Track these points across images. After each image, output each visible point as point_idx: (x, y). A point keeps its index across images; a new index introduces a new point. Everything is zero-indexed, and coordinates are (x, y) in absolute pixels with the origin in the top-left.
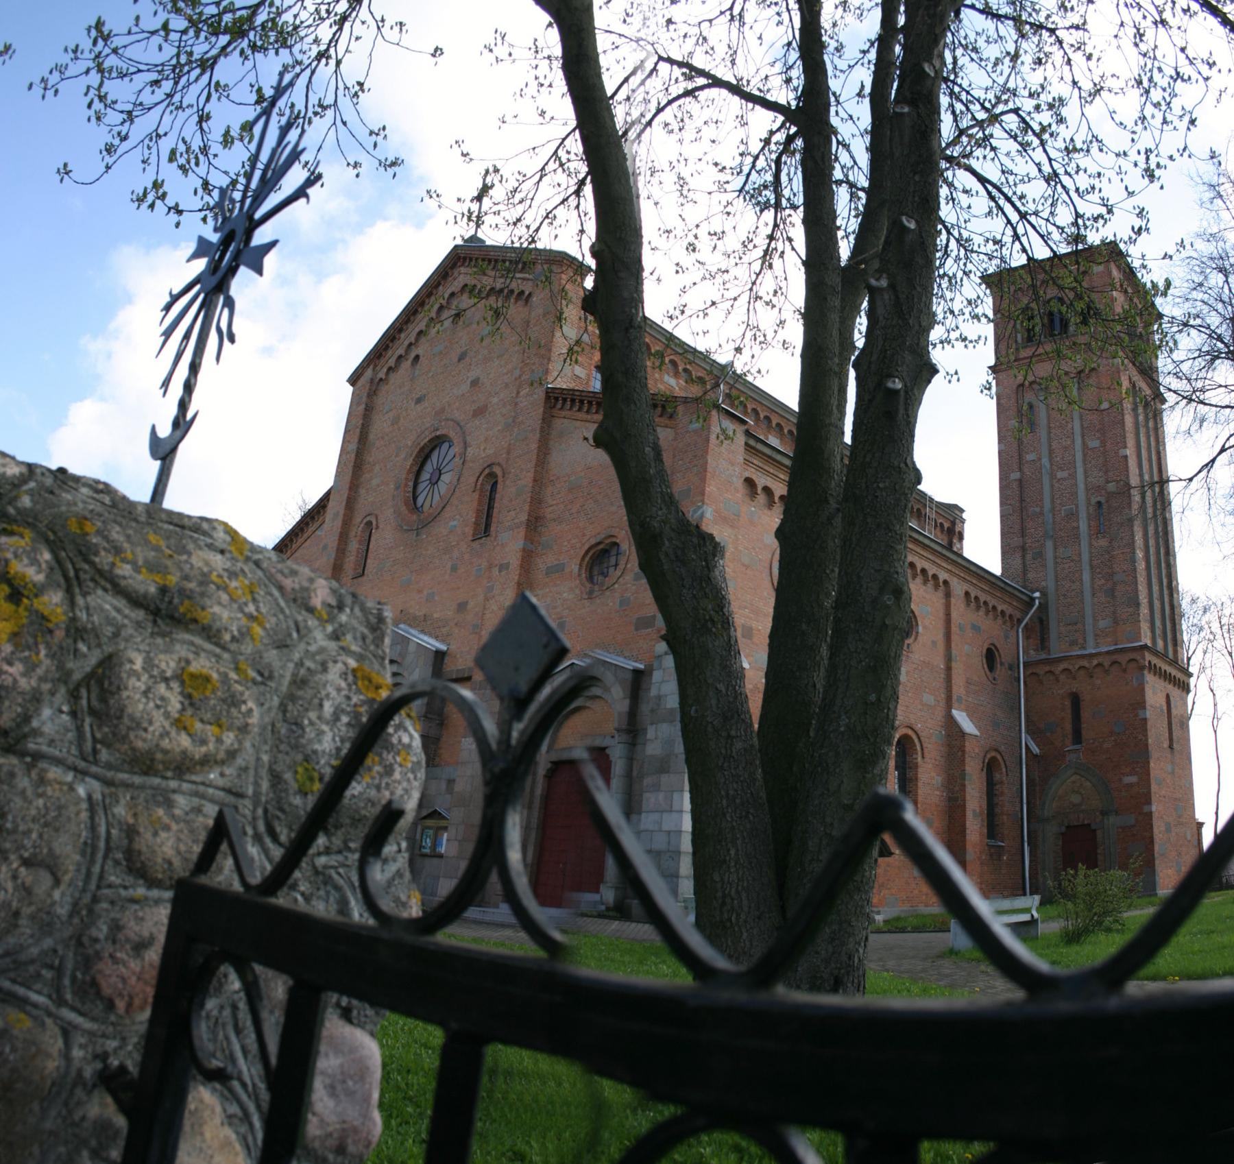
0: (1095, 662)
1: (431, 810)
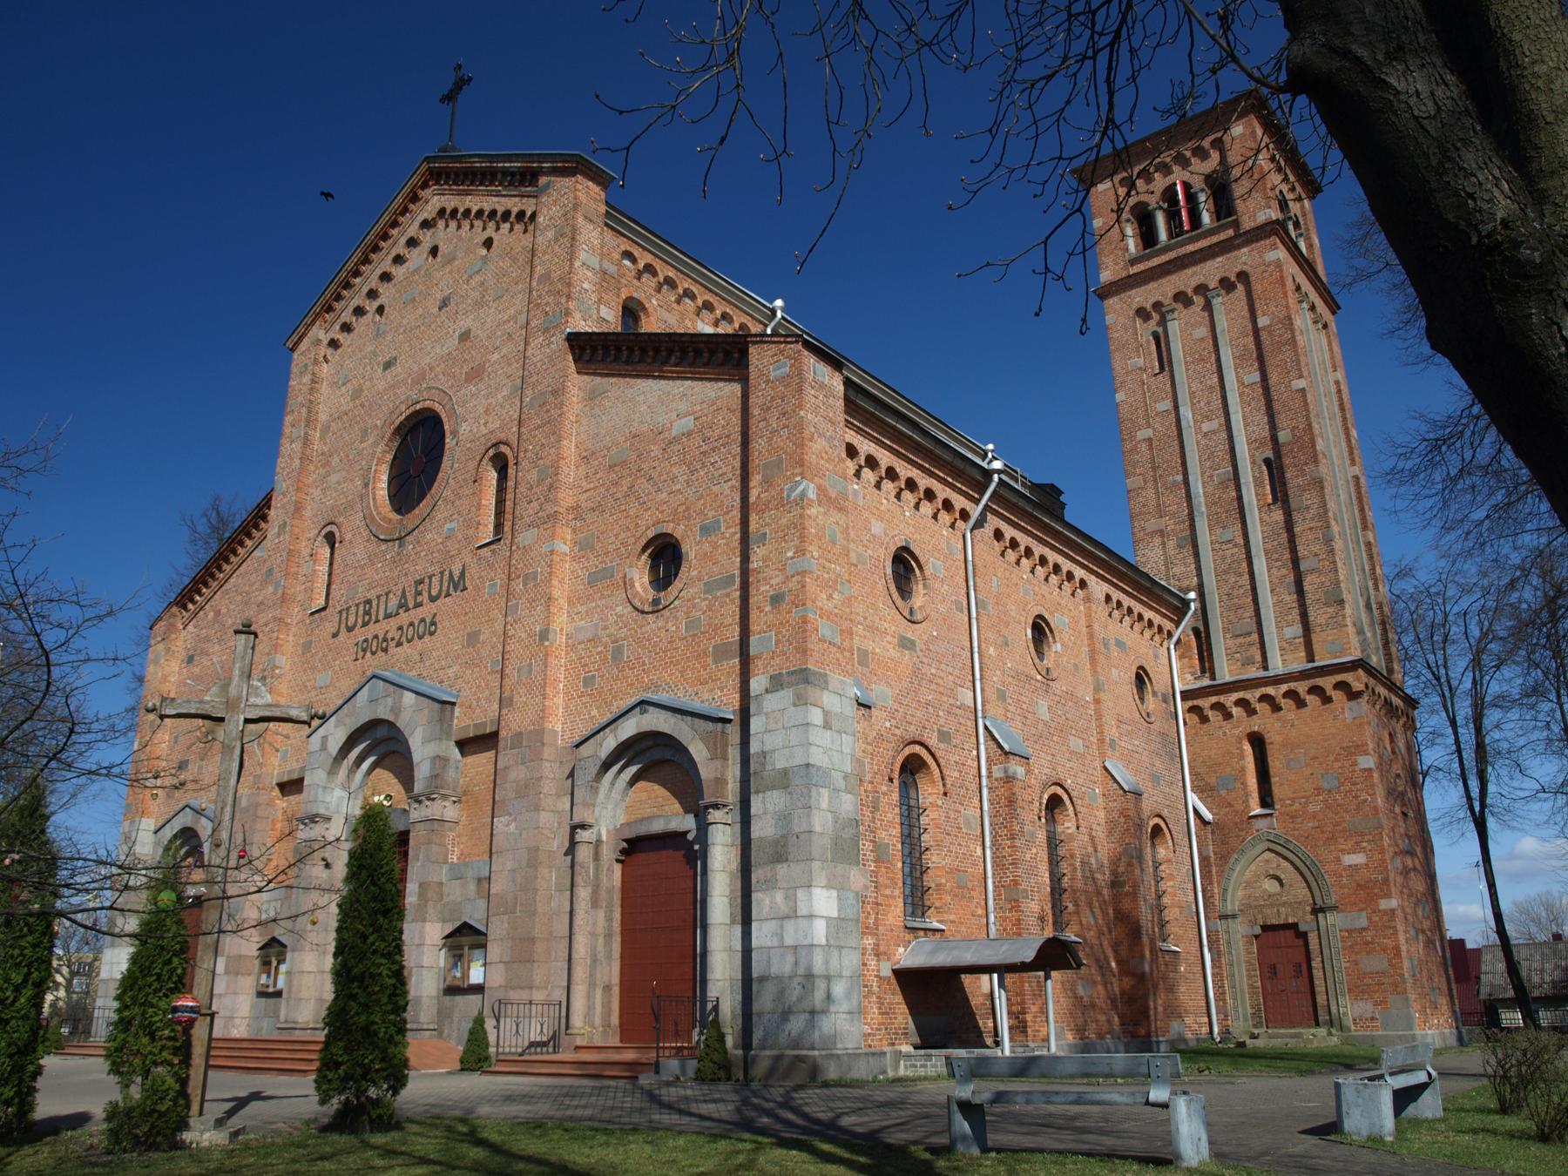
1: (458, 924)
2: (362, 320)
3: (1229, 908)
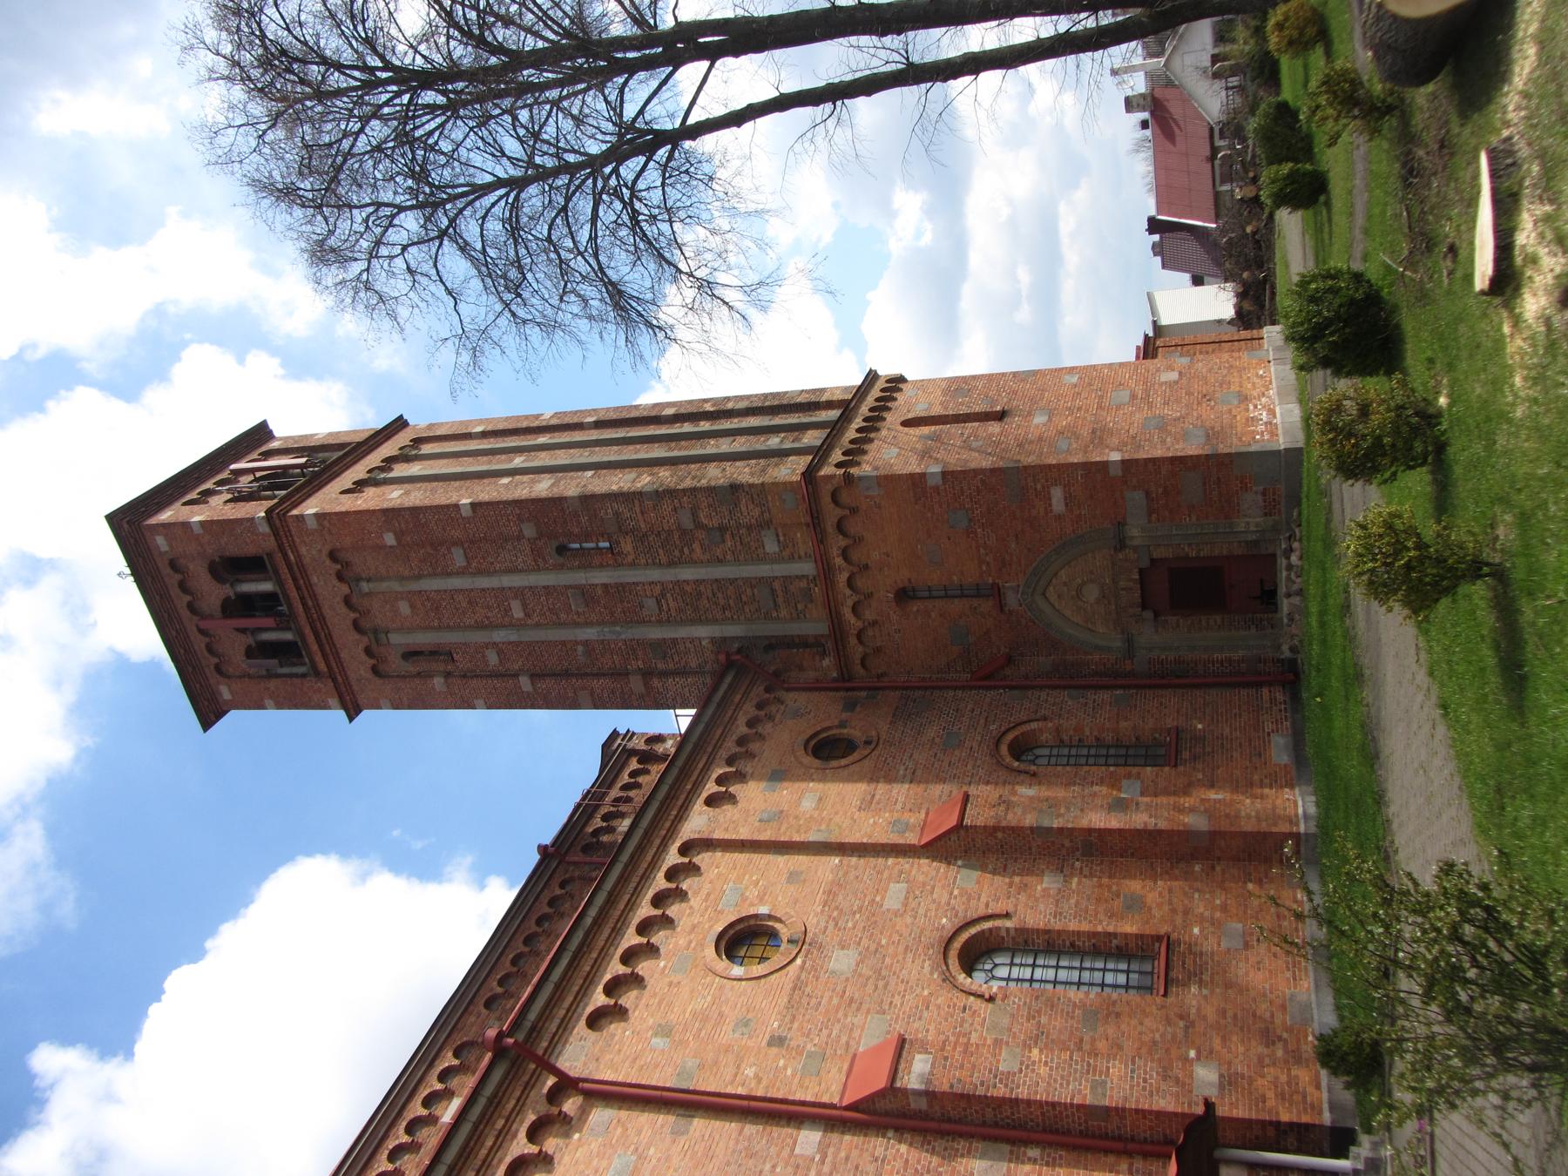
0: (839, 561)
3: (1117, 643)
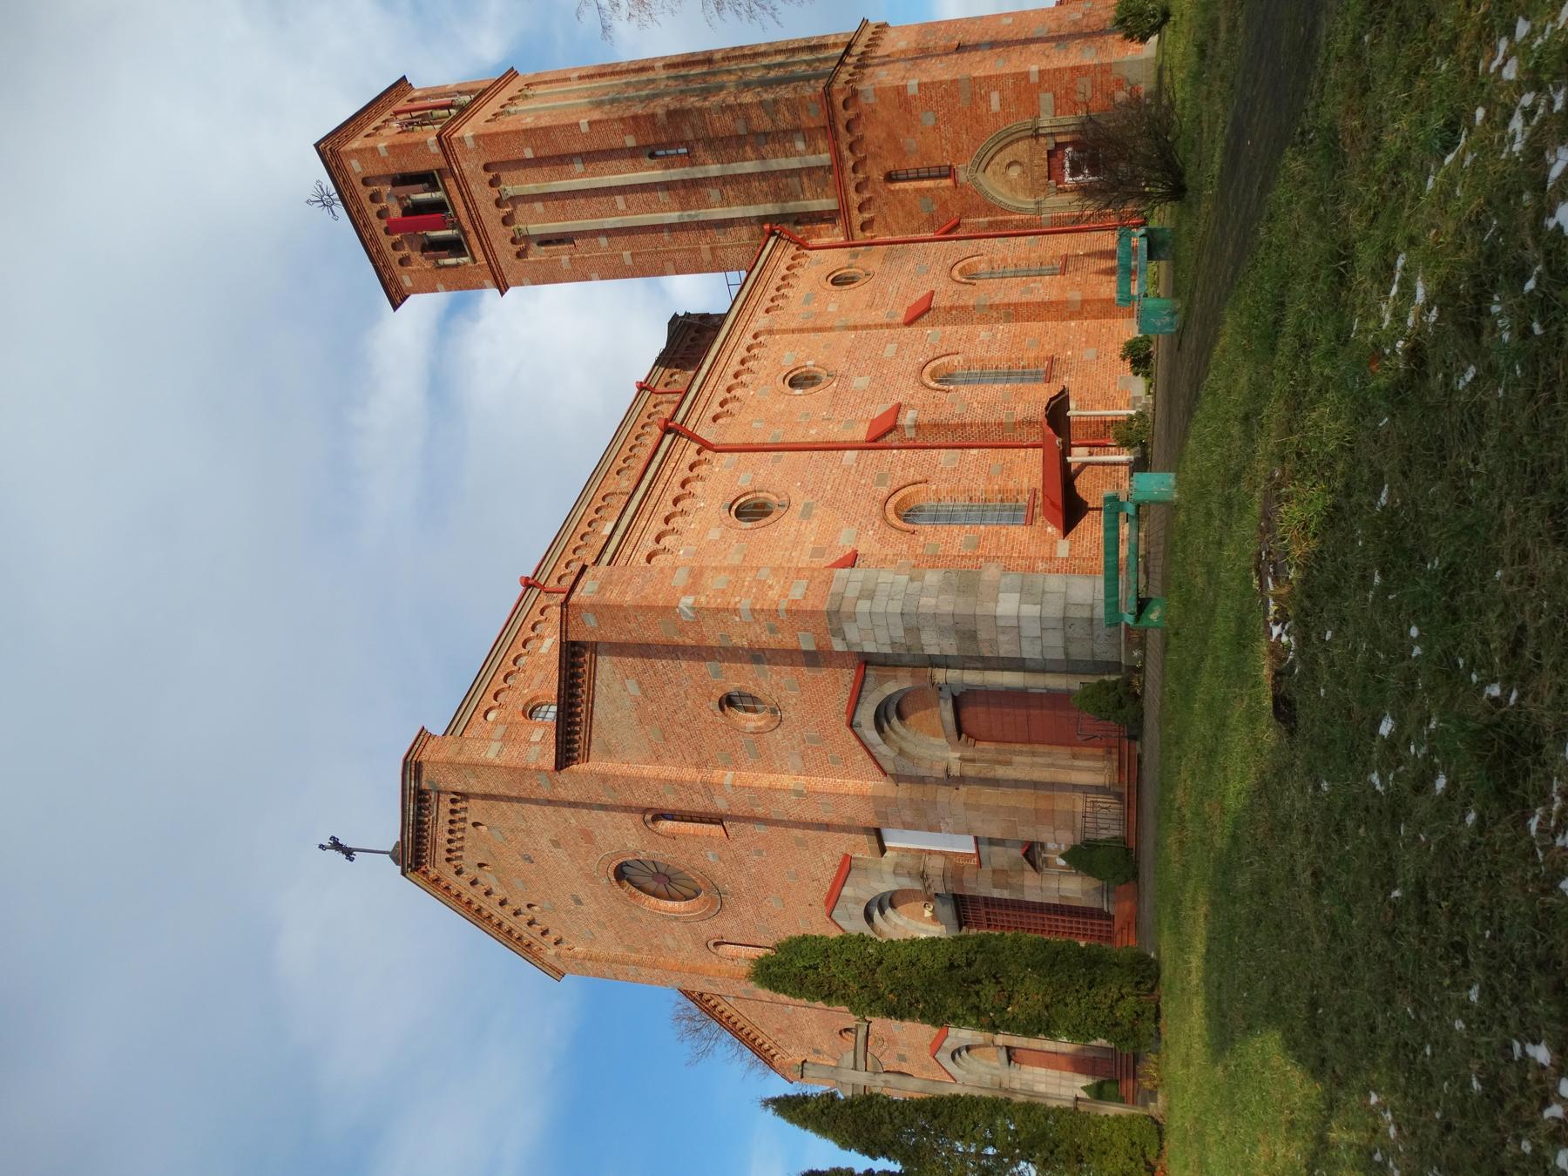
2: (538, 920)
